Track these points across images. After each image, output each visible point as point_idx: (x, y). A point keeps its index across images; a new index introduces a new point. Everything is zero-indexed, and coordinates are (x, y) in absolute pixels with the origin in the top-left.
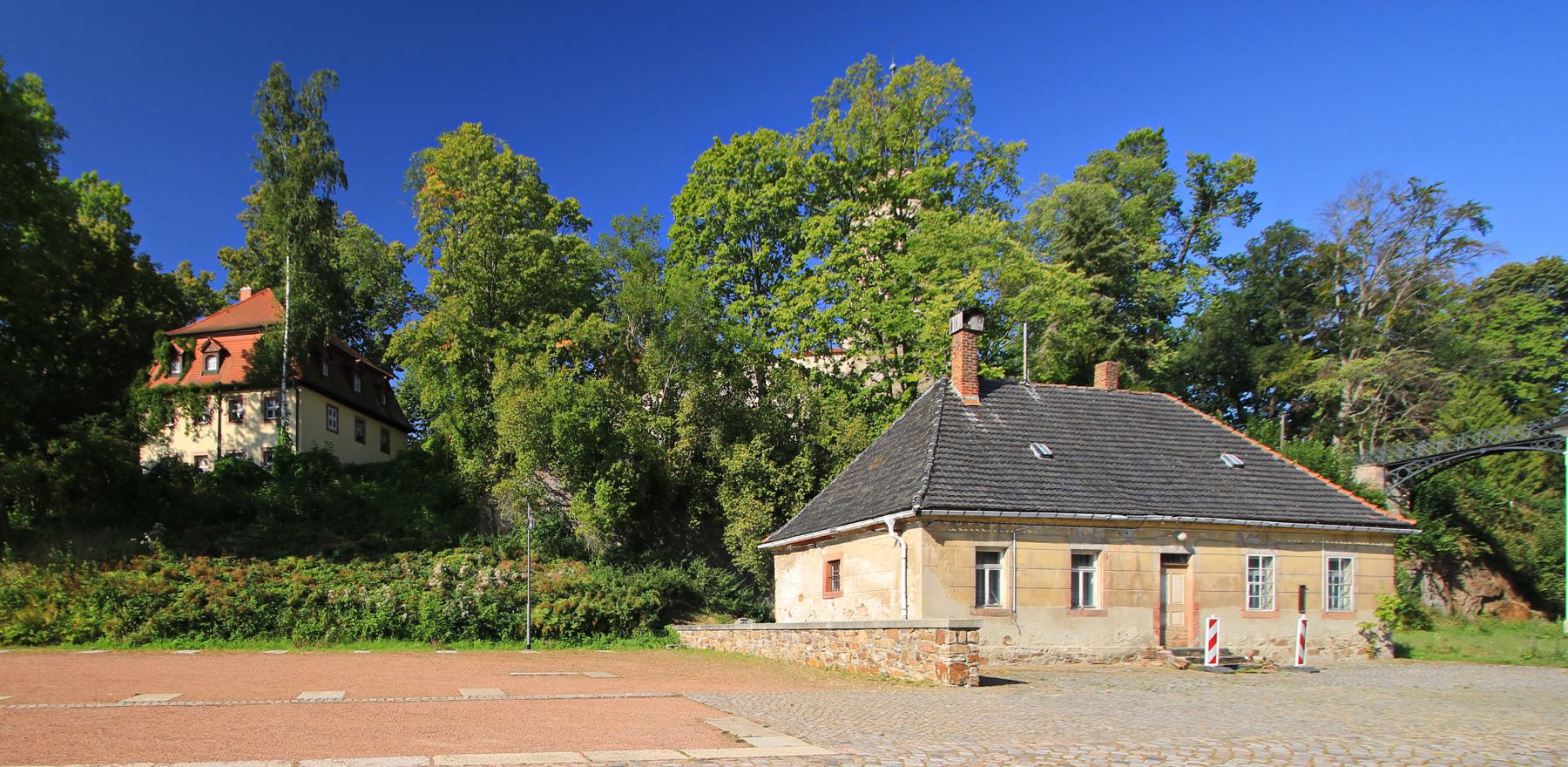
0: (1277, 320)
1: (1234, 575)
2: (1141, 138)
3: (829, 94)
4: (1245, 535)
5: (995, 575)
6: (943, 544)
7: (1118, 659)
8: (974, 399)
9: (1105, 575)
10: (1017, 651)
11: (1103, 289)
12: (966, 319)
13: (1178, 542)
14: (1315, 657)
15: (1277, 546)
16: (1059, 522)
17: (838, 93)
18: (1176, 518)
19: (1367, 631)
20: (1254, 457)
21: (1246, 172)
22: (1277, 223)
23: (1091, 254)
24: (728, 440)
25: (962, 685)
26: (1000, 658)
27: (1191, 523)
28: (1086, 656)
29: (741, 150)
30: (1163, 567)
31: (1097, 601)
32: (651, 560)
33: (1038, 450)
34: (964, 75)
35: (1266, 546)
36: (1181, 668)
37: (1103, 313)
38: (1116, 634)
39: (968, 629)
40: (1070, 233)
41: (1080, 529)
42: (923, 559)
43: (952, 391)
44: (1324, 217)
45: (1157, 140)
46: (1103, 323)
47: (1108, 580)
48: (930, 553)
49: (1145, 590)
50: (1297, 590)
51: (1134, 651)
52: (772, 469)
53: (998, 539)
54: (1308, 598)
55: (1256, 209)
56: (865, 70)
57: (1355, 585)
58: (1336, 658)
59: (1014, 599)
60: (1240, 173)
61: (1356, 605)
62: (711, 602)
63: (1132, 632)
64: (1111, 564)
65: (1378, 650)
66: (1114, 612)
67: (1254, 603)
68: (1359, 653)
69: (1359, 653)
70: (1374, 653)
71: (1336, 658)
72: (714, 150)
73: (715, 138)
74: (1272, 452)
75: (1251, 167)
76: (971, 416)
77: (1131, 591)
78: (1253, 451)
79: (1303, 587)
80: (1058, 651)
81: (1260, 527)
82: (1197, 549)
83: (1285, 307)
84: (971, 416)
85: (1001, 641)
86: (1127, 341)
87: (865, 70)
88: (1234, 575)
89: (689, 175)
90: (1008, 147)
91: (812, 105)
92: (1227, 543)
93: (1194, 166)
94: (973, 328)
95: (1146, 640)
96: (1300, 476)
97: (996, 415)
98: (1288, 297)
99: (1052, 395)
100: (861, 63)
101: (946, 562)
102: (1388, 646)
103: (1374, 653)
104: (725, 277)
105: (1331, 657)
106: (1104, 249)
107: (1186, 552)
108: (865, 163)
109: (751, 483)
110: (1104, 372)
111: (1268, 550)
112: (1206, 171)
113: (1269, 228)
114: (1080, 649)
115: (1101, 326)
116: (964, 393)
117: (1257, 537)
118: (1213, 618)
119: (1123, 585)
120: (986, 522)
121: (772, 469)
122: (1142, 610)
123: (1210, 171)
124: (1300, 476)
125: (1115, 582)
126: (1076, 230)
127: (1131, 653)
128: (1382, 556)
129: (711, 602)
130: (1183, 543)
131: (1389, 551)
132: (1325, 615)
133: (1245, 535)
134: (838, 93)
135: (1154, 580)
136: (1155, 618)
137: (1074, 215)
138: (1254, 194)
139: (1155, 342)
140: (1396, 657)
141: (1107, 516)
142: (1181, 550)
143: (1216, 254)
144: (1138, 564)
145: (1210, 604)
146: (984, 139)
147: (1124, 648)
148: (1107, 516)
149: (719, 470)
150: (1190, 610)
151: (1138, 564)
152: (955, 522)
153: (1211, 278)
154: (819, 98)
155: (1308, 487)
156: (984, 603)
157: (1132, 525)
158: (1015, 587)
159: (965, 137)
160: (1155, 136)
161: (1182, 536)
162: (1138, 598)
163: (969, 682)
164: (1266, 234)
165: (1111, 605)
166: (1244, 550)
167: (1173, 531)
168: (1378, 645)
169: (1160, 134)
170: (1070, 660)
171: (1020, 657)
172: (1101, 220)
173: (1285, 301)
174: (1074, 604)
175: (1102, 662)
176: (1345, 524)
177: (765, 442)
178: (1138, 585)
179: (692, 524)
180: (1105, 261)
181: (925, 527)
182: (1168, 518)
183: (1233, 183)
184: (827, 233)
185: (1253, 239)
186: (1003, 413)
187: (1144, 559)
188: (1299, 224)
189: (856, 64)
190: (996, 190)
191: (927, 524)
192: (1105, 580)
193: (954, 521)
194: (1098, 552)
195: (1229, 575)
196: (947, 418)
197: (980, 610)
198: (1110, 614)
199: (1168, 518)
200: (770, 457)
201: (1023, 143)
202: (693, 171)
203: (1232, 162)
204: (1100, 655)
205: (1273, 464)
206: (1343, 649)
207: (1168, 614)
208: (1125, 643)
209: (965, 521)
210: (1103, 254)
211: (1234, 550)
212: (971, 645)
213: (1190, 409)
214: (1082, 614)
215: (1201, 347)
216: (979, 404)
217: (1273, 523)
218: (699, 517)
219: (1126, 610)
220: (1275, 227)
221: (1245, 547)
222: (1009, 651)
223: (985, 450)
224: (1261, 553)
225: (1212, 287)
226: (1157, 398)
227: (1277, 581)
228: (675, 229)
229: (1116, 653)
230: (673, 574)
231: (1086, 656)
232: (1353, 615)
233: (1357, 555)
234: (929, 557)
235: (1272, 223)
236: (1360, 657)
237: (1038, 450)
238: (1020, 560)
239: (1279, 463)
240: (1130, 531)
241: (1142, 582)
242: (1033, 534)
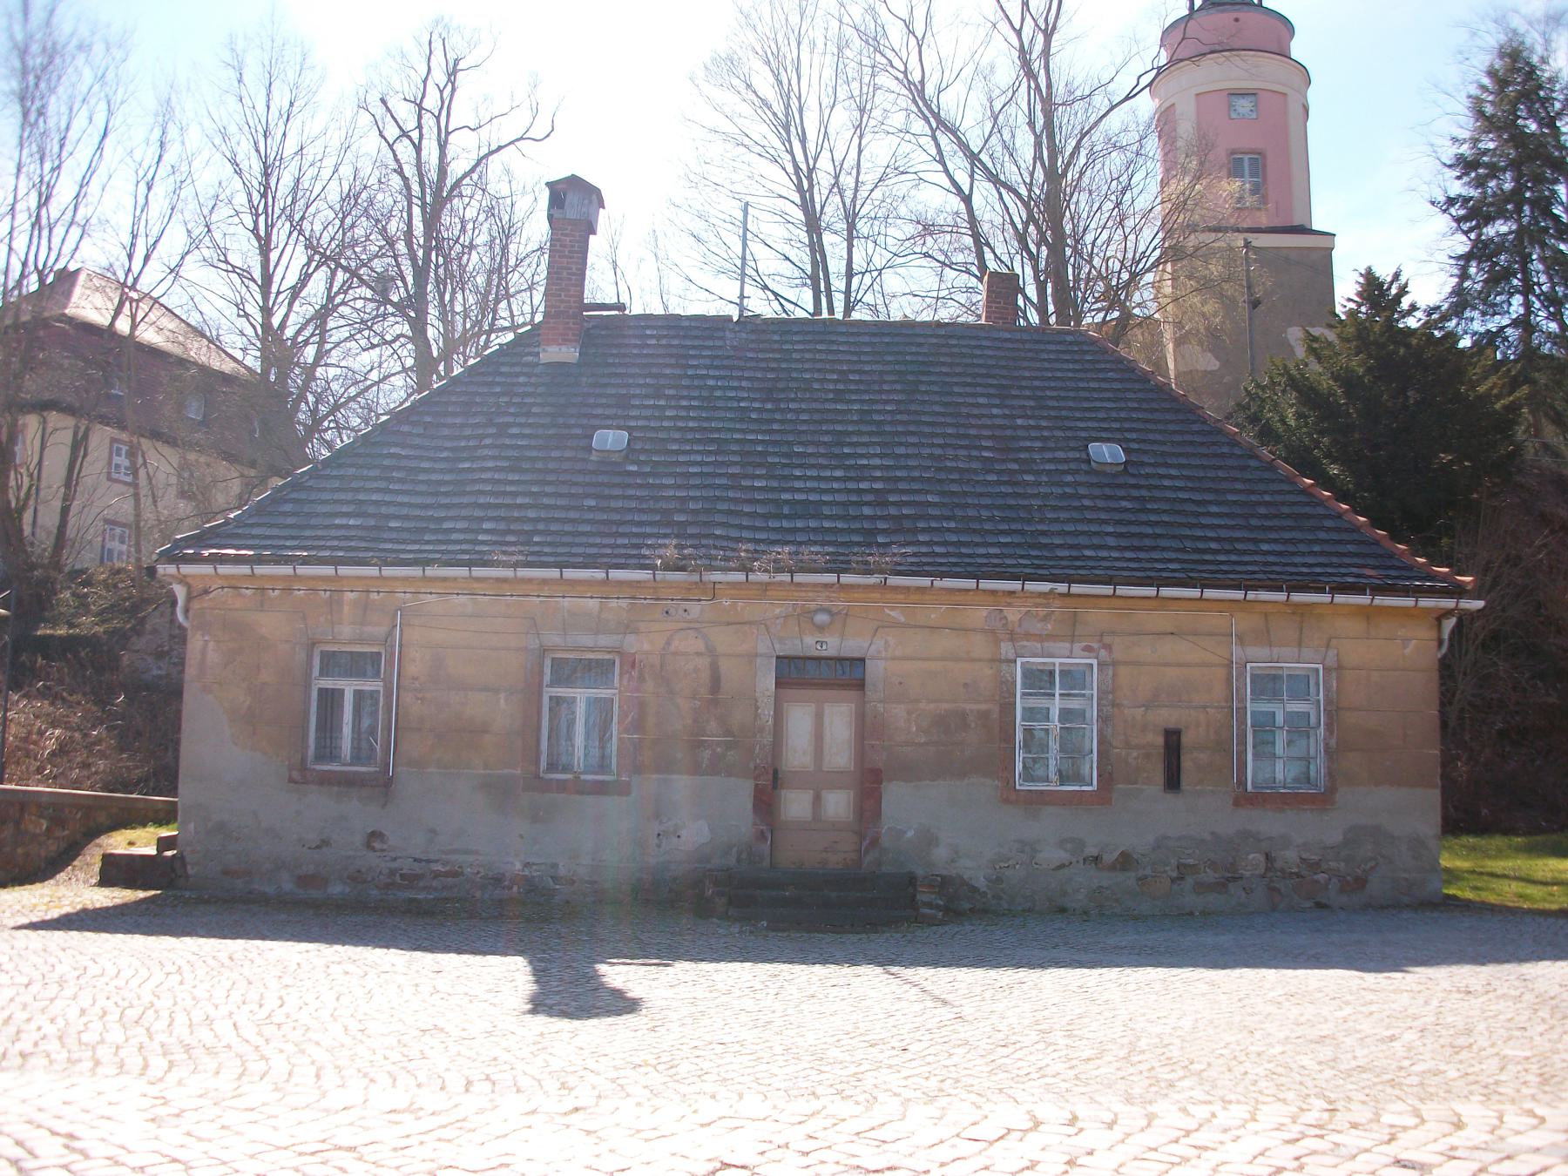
1: (983, 707)
50: (1160, 740)
114: (554, 866)
135: (757, 716)
151: (716, 683)
165: (638, 769)
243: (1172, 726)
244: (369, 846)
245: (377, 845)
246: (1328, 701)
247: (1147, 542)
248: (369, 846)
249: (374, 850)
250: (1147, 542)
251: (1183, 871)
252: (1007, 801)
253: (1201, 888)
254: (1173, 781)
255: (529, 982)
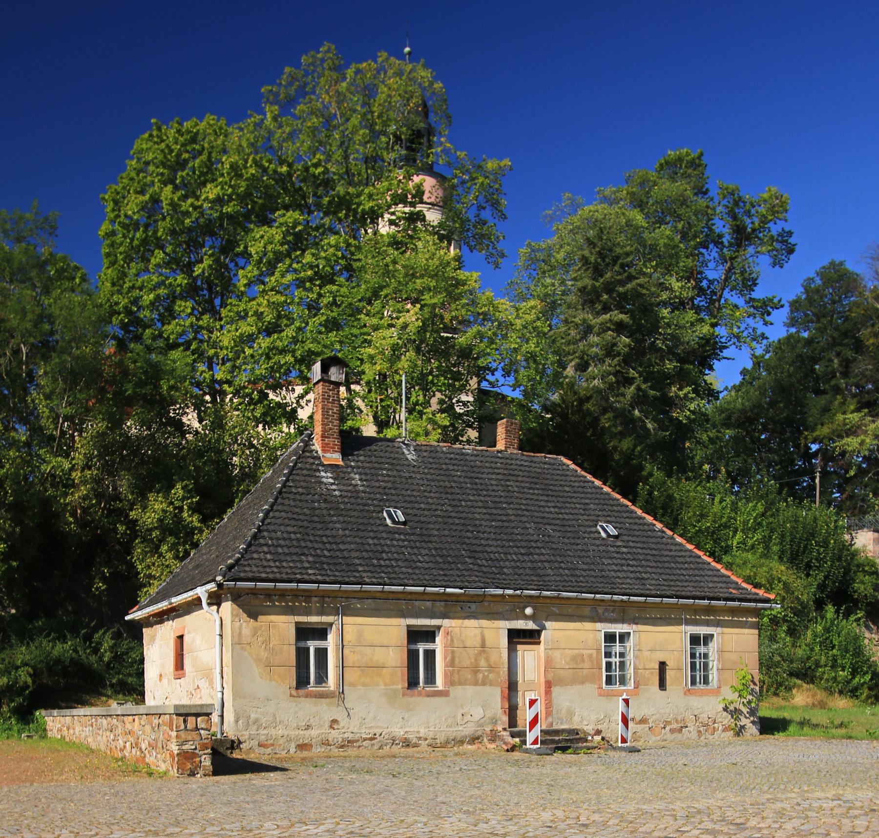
0: (830, 369)
1: (589, 652)
2: (680, 159)
3: (280, 84)
4: (600, 610)
5: (430, 655)
6: (256, 619)
7: (462, 742)
8: (335, 458)
9: (446, 651)
10: (346, 735)
11: (620, 327)
12: (325, 369)
13: (526, 617)
14: (676, 735)
15: (635, 621)
16: (391, 596)
17: (290, 84)
18: (518, 592)
19: (732, 708)
20: (636, 527)
21: (778, 209)
22: (831, 263)
23: (609, 288)
24: (142, 491)
25: (192, 774)
26: (326, 743)
27: (554, 598)
28: (426, 739)
29: (181, 139)
30: (510, 642)
31: (713, 676)
32: (41, 631)
33: (390, 516)
34: (436, 78)
35: (623, 621)
36: (508, 751)
37: (619, 354)
38: (460, 716)
39: (197, 715)
40: (585, 260)
41: (417, 603)
42: (233, 636)
43: (313, 448)
44: (870, 261)
45: (694, 164)
46: (619, 365)
47: (449, 658)
48: (240, 629)
49: (491, 668)
50: (657, 666)
51: (480, 733)
52: (197, 524)
53: (321, 613)
54: (670, 675)
55: (791, 251)
56: (323, 60)
57: (719, 660)
58: (700, 736)
59: (341, 678)
60: (773, 211)
61: (719, 680)
62: (114, 681)
63: (478, 713)
64: (452, 640)
65: (743, 727)
66: (457, 691)
67: (609, 680)
68: (723, 731)
69: (723, 731)
70: (740, 731)
71: (700, 736)
72: (151, 135)
73: (153, 121)
74: (654, 522)
75: (783, 204)
76: (327, 477)
77: (475, 670)
78: (637, 521)
79: (663, 665)
80: (393, 734)
81: (611, 601)
82: (548, 624)
83: (838, 354)
84: (327, 477)
85: (327, 725)
86: (643, 386)
87: (323, 60)
88: (589, 652)
89: (128, 162)
90: (491, 165)
91: (262, 95)
92: (581, 618)
93: (724, 197)
94: (333, 379)
95: (494, 721)
96: (678, 548)
97: (357, 476)
98: (841, 345)
99: (433, 455)
100: (318, 52)
101: (260, 639)
102: (753, 722)
103: (740, 731)
104: (162, 291)
105: (694, 735)
106: (623, 283)
107: (535, 627)
108: (312, 170)
109: (171, 539)
110: (503, 431)
111: (625, 626)
112: (736, 203)
113: (824, 268)
114: (418, 732)
115: (618, 368)
116: (324, 451)
117: (613, 611)
118: (533, 698)
119: (467, 662)
120: (307, 595)
121: (197, 524)
122: (488, 689)
123: (741, 205)
124: (678, 548)
125: (457, 661)
126: (592, 259)
127: (477, 734)
128: (746, 631)
129: (114, 681)
130: (532, 618)
131: (752, 626)
132: (688, 692)
133: (600, 610)
134: (290, 84)
135: (501, 657)
136: (503, 697)
137: (590, 242)
138: (790, 234)
139: (680, 389)
140: (761, 733)
141: (442, 590)
142: (531, 625)
143: (754, 295)
144: (483, 641)
145: (561, 682)
146: (461, 154)
147: (468, 730)
148: (442, 590)
149: (132, 524)
150: (543, 689)
151: (483, 641)
152: (310, 597)
153: (750, 321)
154: (270, 88)
155: (679, 560)
156: (309, 683)
157: (475, 599)
158: (342, 666)
159: (439, 149)
160: (694, 159)
161: (529, 611)
162: (484, 675)
163: (201, 772)
164: (821, 274)
165: (452, 684)
166: (599, 626)
167: (522, 605)
168: (744, 721)
169: (699, 158)
170: (407, 743)
171: (349, 742)
172: (618, 250)
173: (838, 349)
174: (413, 683)
175: (445, 744)
176: (703, 598)
177: (189, 491)
178: (483, 663)
179: (97, 589)
180: (624, 297)
181: (234, 600)
182: (510, 592)
183: (764, 221)
184: (269, 248)
185: (809, 279)
186: (366, 474)
187: (489, 636)
188: (850, 266)
189: (312, 53)
190: (482, 212)
191: (237, 597)
192: (445, 658)
193: (269, 594)
194: (439, 627)
195: (585, 652)
196: (297, 478)
197: (302, 692)
198: (451, 694)
199: (510, 592)
200: (194, 509)
201: (506, 162)
202: (132, 158)
203: (765, 196)
204: (441, 738)
205: (654, 534)
206: (708, 726)
207: (520, 694)
208: (470, 725)
209: (283, 594)
210: (621, 289)
211: (588, 625)
212: (202, 732)
213: (583, 473)
214: (420, 694)
215: (763, 394)
216: (341, 463)
217: (625, 598)
218: (104, 579)
219: (470, 690)
220: (829, 268)
221: (601, 622)
222: (335, 735)
223: (329, 515)
224: (618, 628)
225: (751, 330)
226: (552, 461)
227: (635, 657)
228: (105, 227)
229: (459, 736)
230: (63, 649)
231: (426, 739)
232: (717, 691)
233: (719, 629)
234: (240, 634)
235: (826, 263)
236: (724, 734)
237: (390, 516)
238: (347, 637)
239: (659, 533)
240: (473, 606)
241: (487, 659)
242: (362, 609)
243: (661, 660)
244: (331, 727)
245: (335, 727)
246: (718, 648)
247: (639, 545)
248: (331, 727)
249: (334, 729)
250: (639, 545)
251: (667, 723)
252: (600, 695)
253: (672, 731)
254: (662, 685)
255: (571, 713)
